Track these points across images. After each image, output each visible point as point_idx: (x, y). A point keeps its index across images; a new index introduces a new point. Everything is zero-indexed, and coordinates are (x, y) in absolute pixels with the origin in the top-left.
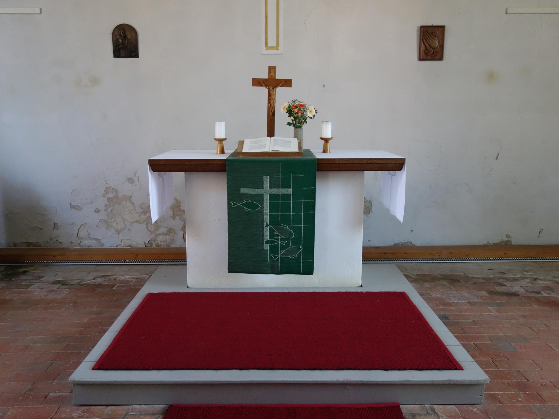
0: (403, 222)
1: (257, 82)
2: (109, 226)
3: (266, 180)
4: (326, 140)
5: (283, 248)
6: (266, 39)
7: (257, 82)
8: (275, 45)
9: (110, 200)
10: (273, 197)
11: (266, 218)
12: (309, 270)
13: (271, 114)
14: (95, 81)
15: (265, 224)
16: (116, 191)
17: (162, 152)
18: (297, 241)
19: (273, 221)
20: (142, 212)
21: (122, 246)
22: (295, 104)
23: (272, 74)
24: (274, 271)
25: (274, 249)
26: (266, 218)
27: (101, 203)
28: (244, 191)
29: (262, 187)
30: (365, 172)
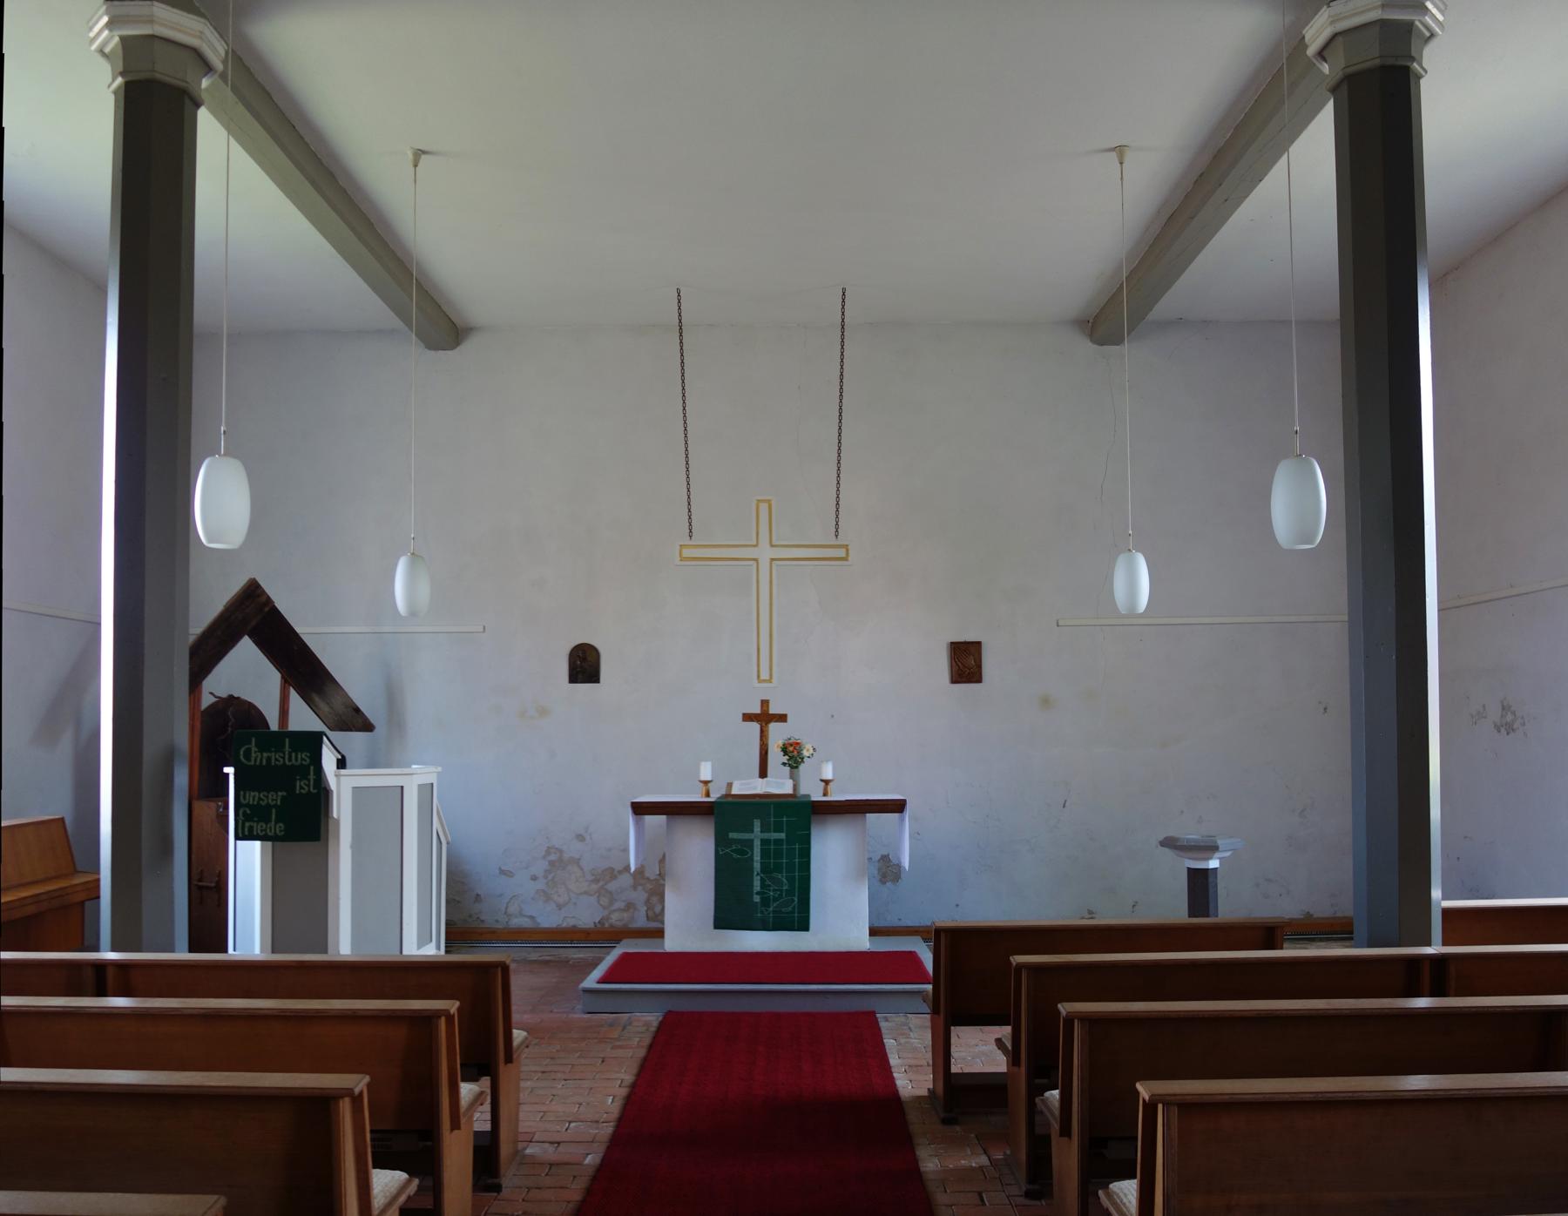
0: (909, 866)
1: (748, 717)
2: (548, 898)
3: (757, 824)
4: (827, 782)
5: (775, 900)
6: (758, 671)
7: (748, 717)
8: (768, 678)
9: (552, 863)
10: (764, 842)
11: (757, 866)
12: (804, 926)
13: (764, 752)
14: (543, 712)
15: (755, 873)
16: (561, 851)
17: (635, 798)
18: (790, 892)
19: (765, 869)
20: (592, 881)
21: (564, 925)
22: (791, 741)
23: (765, 708)
24: (765, 927)
25: (765, 902)
26: (757, 866)
27: (540, 867)
28: (733, 835)
29: (752, 831)
30: (868, 815)
